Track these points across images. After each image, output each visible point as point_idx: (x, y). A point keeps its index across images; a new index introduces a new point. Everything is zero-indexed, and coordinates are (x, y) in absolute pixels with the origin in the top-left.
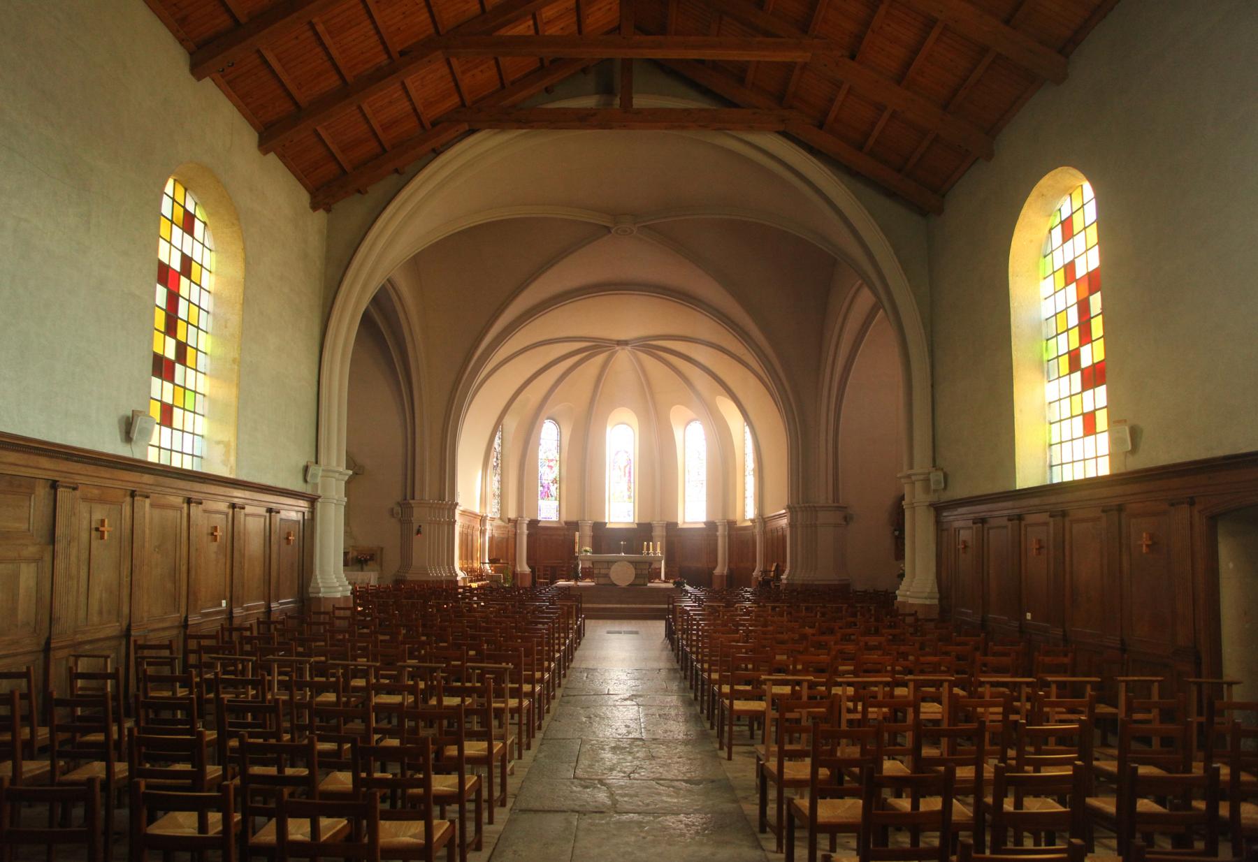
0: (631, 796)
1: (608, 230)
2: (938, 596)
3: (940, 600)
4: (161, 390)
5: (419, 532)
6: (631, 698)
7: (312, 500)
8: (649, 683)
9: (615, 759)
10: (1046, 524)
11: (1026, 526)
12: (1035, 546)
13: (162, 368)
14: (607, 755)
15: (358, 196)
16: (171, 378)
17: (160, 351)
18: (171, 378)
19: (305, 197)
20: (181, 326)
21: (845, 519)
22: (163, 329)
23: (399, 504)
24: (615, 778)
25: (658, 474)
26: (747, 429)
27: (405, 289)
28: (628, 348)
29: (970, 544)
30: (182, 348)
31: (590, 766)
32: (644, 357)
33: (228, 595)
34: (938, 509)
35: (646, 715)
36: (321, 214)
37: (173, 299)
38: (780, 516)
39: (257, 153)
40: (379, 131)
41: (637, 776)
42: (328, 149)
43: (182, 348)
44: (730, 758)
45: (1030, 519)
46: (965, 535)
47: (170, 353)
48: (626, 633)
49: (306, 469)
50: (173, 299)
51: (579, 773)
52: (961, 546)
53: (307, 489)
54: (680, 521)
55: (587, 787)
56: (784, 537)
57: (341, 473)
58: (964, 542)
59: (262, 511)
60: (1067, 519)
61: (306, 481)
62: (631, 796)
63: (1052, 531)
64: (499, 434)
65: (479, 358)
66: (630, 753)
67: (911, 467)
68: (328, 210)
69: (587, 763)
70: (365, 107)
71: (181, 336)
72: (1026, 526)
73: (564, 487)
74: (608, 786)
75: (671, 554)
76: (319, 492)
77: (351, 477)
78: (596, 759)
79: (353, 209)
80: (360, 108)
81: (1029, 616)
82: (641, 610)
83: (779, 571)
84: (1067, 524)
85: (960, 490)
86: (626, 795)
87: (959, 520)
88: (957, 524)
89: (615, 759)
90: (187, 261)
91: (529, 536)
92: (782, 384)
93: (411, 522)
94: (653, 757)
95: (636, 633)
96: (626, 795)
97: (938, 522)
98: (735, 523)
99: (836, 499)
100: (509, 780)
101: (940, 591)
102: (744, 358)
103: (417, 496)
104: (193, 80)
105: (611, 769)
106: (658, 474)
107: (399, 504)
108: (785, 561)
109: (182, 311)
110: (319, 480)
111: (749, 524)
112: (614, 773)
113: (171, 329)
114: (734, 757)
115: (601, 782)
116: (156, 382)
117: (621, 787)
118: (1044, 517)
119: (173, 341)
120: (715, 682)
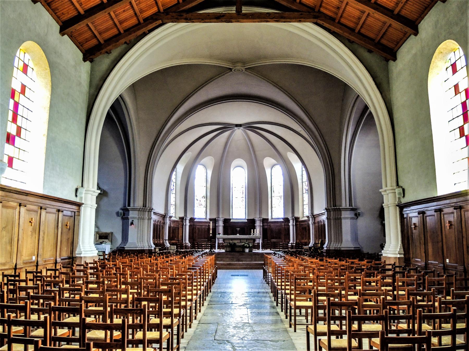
0: (242, 347)
1: (231, 69)
2: (403, 252)
3: (404, 254)
4: (9, 149)
5: (132, 224)
6: (244, 305)
7: (79, 205)
8: (253, 299)
9: (235, 332)
10: (453, 213)
11: (444, 214)
12: (448, 225)
13: (10, 139)
14: (231, 331)
15: (106, 55)
16: (13, 144)
17: (9, 131)
18: (13, 144)
19: (81, 55)
20: (19, 118)
21: (356, 215)
22: (11, 120)
23: (122, 209)
24: (235, 340)
25: (258, 192)
26: (304, 169)
27: (128, 100)
28: (242, 128)
29: (417, 225)
30: (19, 129)
31: (222, 335)
32: (250, 133)
33: (36, 253)
34: (401, 207)
35: (251, 313)
36: (88, 63)
37: (16, 105)
38: (322, 214)
39: (59, 35)
40: (118, 24)
41: (246, 339)
42: (93, 33)
43: (19, 129)
44: (295, 331)
45: (446, 210)
46: (415, 220)
47: (14, 132)
48: (241, 275)
49: (77, 190)
50: (16, 105)
51: (217, 338)
52: (413, 226)
53: (77, 200)
54: (270, 218)
55: (221, 344)
56: (324, 225)
57: (94, 192)
58: (414, 224)
59: (54, 211)
60: (462, 210)
61: (76, 196)
62: (242, 347)
63: (455, 216)
64: (174, 173)
65: (164, 136)
66: (243, 329)
67: (386, 187)
68: (91, 61)
69: (221, 333)
70: (112, 14)
71: (19, 123)
72: (444, 214)
73: (208, 201)
74: (232, 343)
75: (265, 232)
76: (83, 202)
77: (100, 194)
78: (225, 332)
79: (104, 61)
80: (109, 14)
81: (448, 261)
82: (248, 264)
83: (323, 243)
84: (463, 213)
85: (409, 198)
86: (240, 347)
87: (412, 213)
88: (410, 215)
89: (235, 332)
90: (23, 87)
91: (190, 226)
92: (320, 144)
93: (128, 219)
94: (254, 331)
95: (247, 276)
96: (240, 347)
97: (402, 215)
98: (299, 218)
99: (350, 204)
100: (182, 341)
101: (404, 250)
102: (301, 133)
103: (132, 205)
104: (32, 3)
105: (233, 336)
106: (258, 192)
107: (122, 209)
108: (325, 238)
109: (20, 111)
110: (83, 196)
111: (306, 219)
112: (235, 338)
113: (15, 120)
114: (297, 331)
115: (228, 341)
116: (7, 145)
117: (238, 343)
118: (451, 210)
119: (16, 126)
120: (288, 294)
